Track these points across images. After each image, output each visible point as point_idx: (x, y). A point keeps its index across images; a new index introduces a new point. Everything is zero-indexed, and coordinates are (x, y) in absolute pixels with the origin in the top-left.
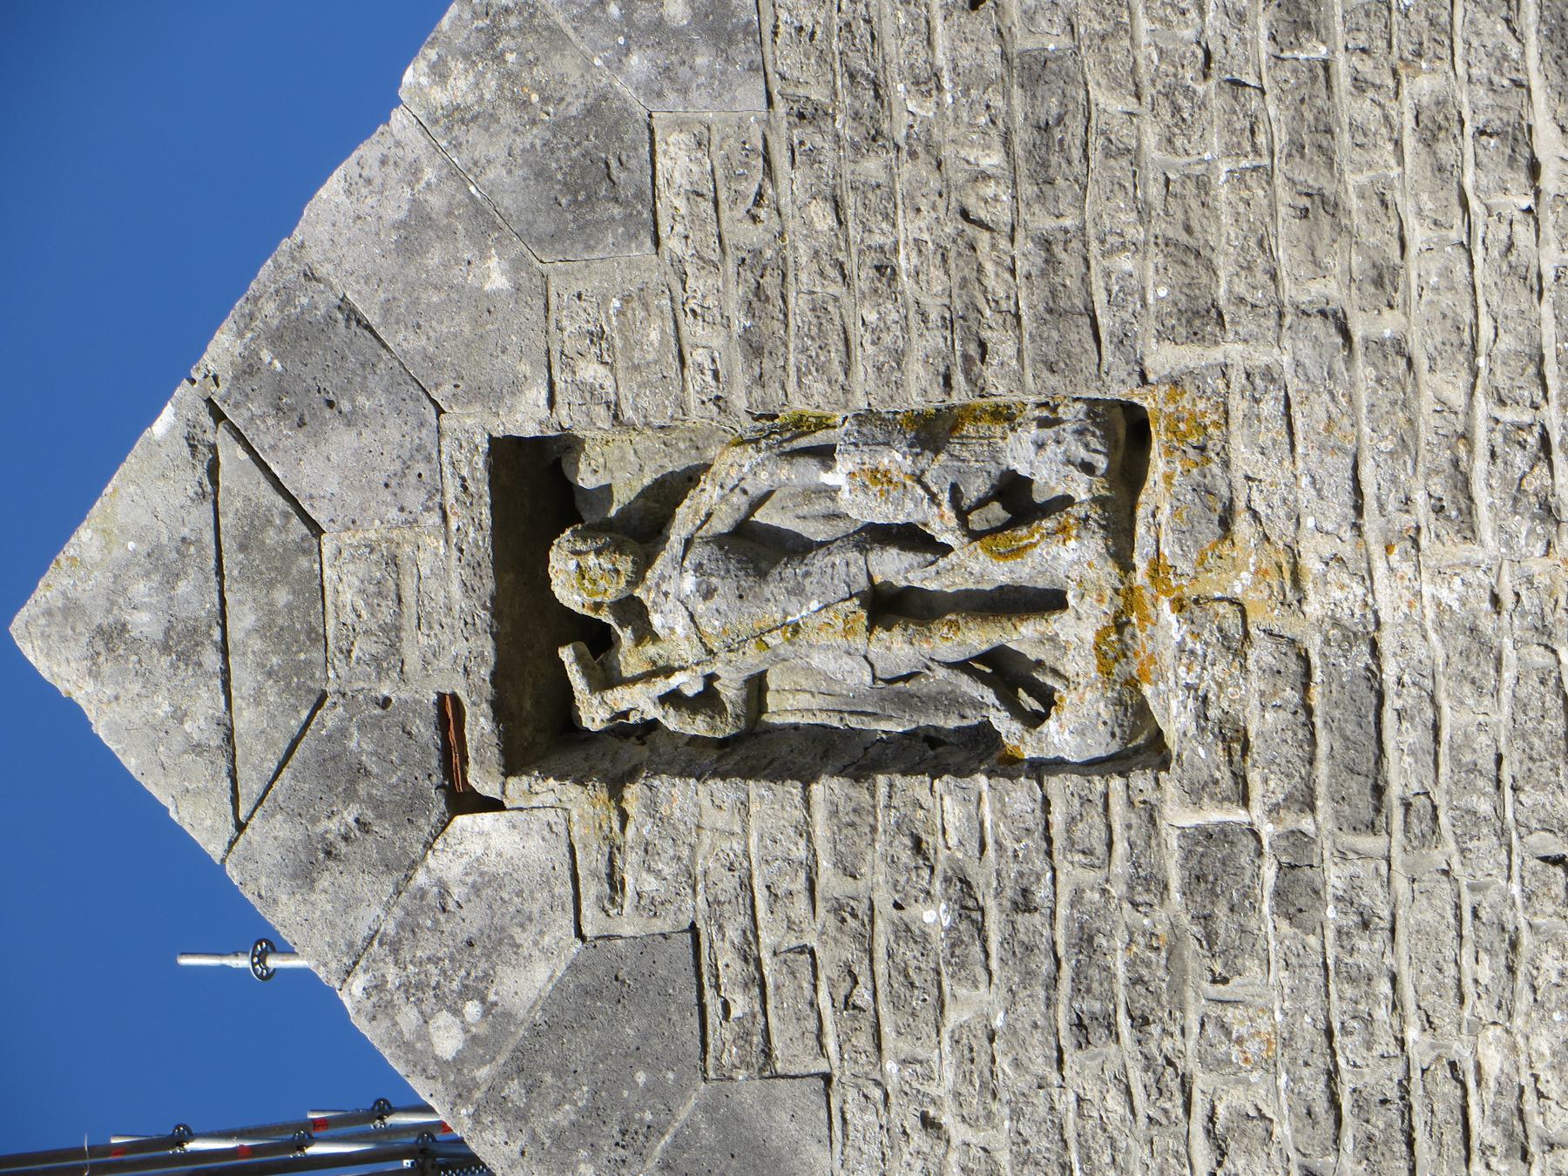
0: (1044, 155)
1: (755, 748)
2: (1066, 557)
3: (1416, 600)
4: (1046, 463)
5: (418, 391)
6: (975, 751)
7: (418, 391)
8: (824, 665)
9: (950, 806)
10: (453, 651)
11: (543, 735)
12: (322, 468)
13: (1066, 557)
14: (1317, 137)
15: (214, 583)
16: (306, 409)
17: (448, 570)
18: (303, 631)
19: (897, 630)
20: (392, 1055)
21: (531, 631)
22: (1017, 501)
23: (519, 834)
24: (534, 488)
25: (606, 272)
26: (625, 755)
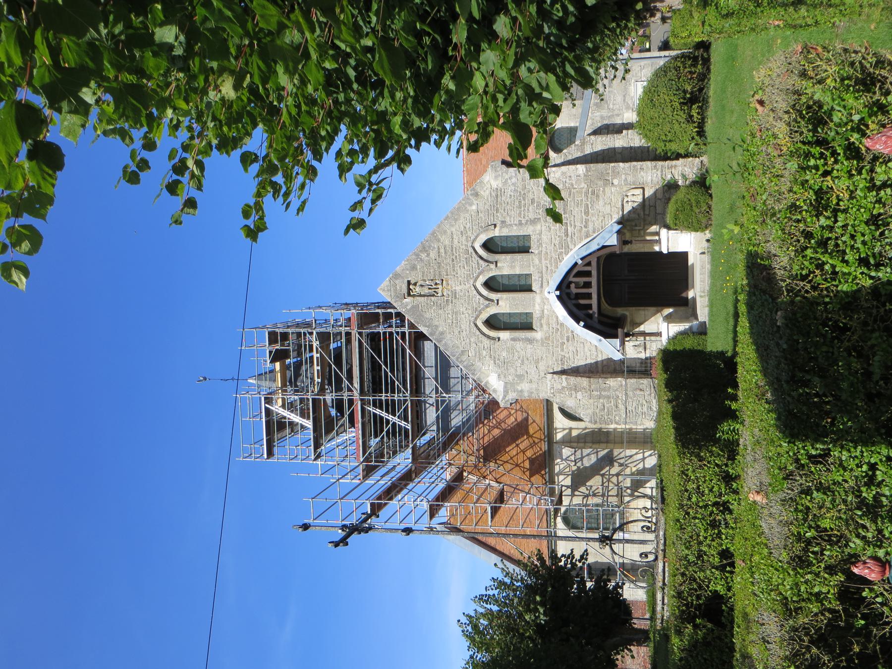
0: (439, 267)
1: (421, 296)
2: (440, 286)
3: (458, 288)
4: (438, 282)
5: (403, 278)
6: (433, 295)
7: (403, 278)
8: (426, 291)
9: (433, 298)
10: (405, 291)
11: (409, 295)
12: (397, 282)
13: (440, 286)
14: (454, 267)
15: (732, 322)
16: (396, 279)
17: (405, 286)
18: (396, 290)
19: (709, 349)
20: (521, 267)
21: (409, 289)
22: (436, 284)
23: (409, 300)
24: (409, 283)
25: (413, 273)
26: (414, 296)
